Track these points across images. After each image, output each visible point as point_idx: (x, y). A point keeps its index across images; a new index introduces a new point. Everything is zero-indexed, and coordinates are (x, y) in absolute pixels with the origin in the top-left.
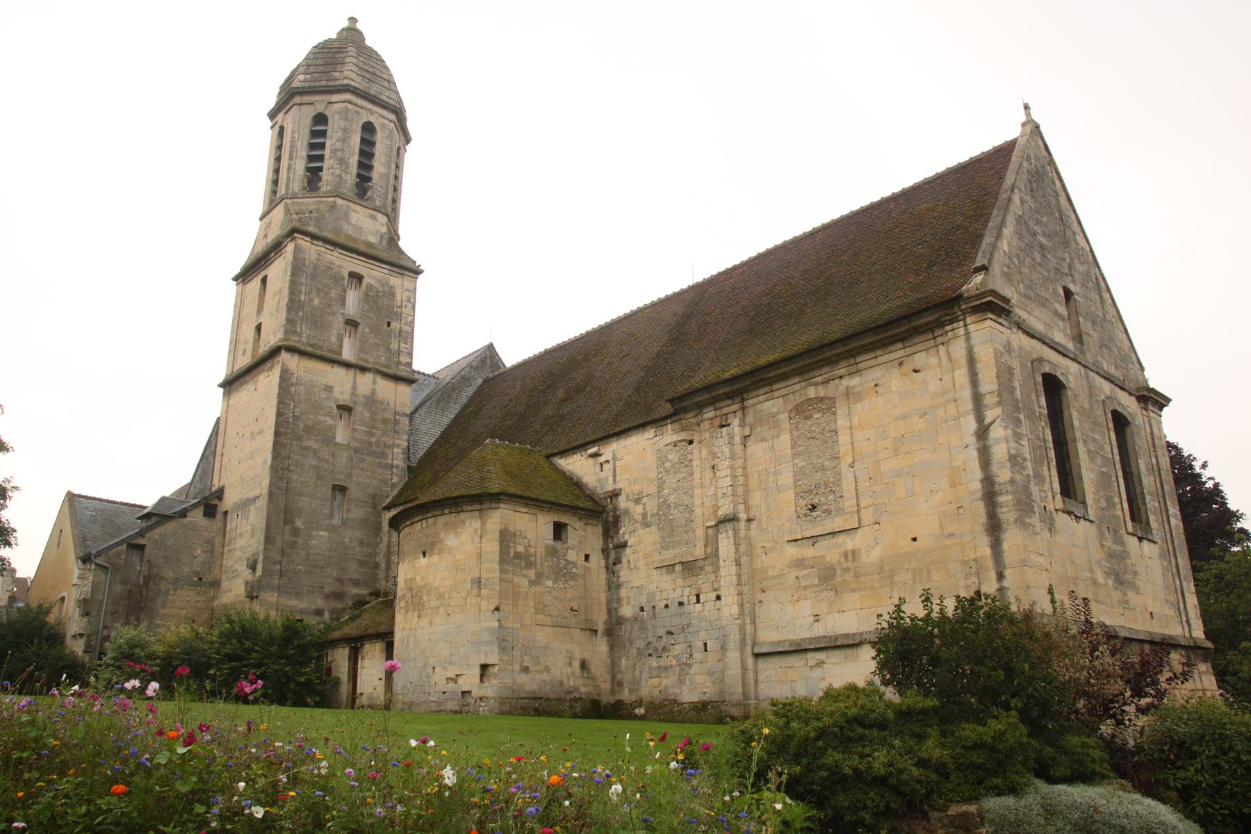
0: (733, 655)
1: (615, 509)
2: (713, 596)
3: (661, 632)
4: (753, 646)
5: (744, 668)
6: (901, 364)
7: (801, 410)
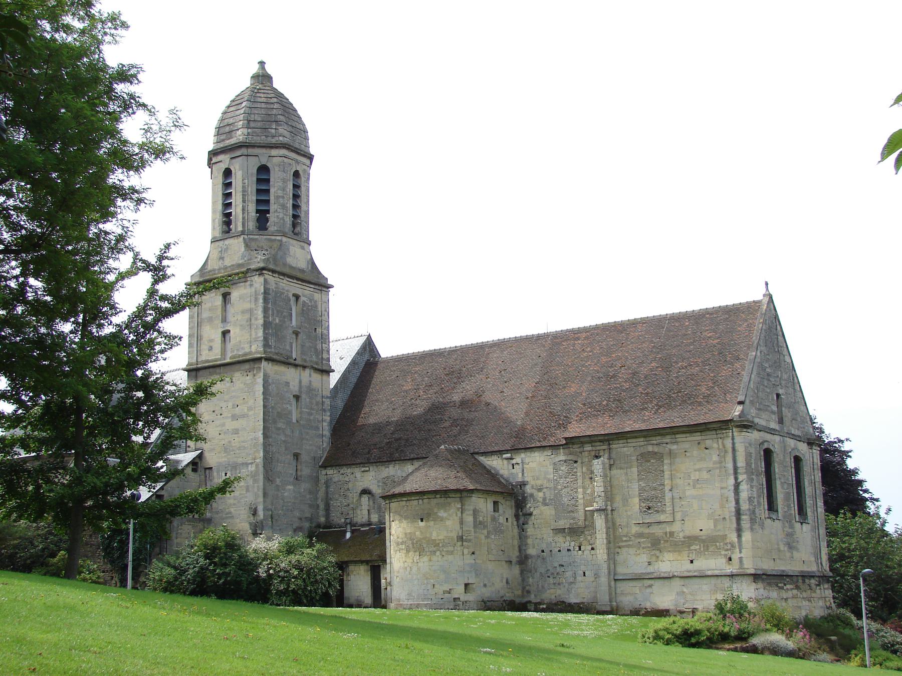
0: (604, 580)
1: (524, 492)
2: (590, 547)
3: (556, 565)
4: (615, 575)
5: (610, 586)
6: (699, 443)
7: (645, 457)
